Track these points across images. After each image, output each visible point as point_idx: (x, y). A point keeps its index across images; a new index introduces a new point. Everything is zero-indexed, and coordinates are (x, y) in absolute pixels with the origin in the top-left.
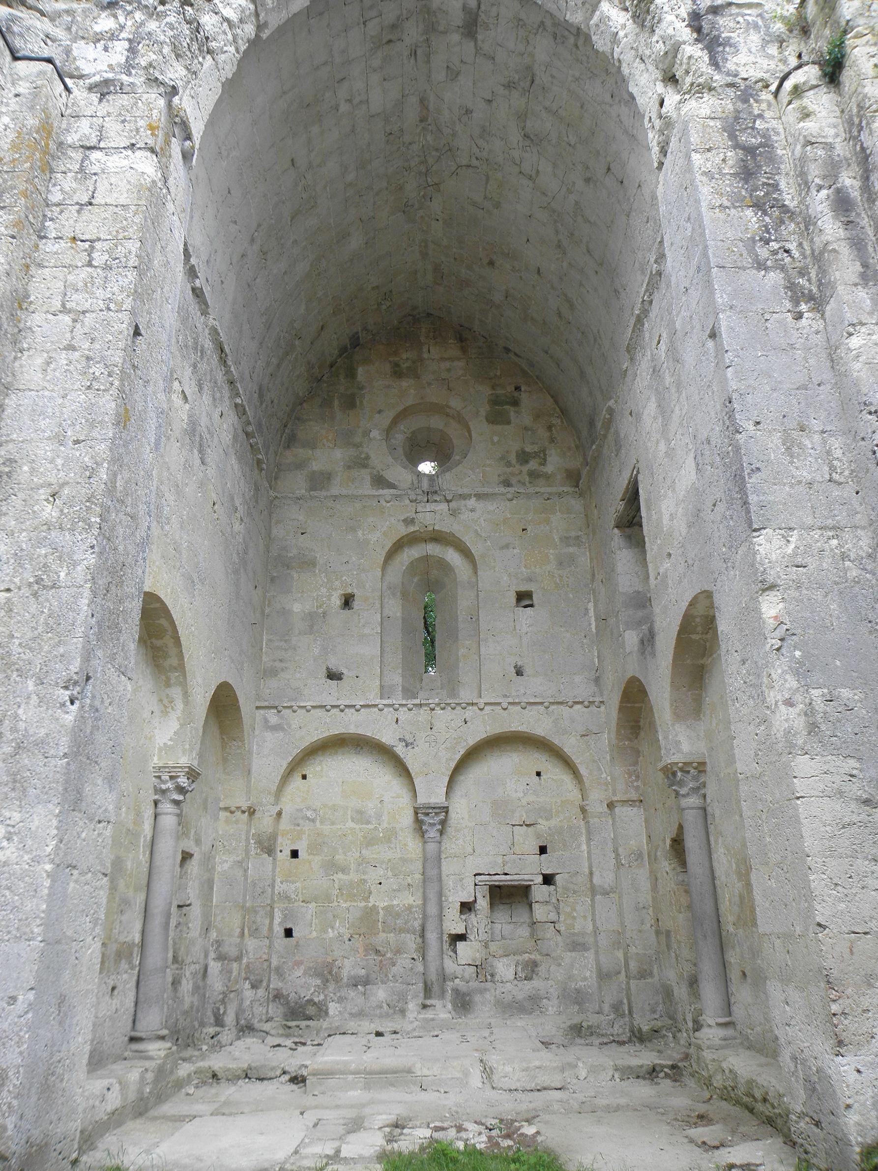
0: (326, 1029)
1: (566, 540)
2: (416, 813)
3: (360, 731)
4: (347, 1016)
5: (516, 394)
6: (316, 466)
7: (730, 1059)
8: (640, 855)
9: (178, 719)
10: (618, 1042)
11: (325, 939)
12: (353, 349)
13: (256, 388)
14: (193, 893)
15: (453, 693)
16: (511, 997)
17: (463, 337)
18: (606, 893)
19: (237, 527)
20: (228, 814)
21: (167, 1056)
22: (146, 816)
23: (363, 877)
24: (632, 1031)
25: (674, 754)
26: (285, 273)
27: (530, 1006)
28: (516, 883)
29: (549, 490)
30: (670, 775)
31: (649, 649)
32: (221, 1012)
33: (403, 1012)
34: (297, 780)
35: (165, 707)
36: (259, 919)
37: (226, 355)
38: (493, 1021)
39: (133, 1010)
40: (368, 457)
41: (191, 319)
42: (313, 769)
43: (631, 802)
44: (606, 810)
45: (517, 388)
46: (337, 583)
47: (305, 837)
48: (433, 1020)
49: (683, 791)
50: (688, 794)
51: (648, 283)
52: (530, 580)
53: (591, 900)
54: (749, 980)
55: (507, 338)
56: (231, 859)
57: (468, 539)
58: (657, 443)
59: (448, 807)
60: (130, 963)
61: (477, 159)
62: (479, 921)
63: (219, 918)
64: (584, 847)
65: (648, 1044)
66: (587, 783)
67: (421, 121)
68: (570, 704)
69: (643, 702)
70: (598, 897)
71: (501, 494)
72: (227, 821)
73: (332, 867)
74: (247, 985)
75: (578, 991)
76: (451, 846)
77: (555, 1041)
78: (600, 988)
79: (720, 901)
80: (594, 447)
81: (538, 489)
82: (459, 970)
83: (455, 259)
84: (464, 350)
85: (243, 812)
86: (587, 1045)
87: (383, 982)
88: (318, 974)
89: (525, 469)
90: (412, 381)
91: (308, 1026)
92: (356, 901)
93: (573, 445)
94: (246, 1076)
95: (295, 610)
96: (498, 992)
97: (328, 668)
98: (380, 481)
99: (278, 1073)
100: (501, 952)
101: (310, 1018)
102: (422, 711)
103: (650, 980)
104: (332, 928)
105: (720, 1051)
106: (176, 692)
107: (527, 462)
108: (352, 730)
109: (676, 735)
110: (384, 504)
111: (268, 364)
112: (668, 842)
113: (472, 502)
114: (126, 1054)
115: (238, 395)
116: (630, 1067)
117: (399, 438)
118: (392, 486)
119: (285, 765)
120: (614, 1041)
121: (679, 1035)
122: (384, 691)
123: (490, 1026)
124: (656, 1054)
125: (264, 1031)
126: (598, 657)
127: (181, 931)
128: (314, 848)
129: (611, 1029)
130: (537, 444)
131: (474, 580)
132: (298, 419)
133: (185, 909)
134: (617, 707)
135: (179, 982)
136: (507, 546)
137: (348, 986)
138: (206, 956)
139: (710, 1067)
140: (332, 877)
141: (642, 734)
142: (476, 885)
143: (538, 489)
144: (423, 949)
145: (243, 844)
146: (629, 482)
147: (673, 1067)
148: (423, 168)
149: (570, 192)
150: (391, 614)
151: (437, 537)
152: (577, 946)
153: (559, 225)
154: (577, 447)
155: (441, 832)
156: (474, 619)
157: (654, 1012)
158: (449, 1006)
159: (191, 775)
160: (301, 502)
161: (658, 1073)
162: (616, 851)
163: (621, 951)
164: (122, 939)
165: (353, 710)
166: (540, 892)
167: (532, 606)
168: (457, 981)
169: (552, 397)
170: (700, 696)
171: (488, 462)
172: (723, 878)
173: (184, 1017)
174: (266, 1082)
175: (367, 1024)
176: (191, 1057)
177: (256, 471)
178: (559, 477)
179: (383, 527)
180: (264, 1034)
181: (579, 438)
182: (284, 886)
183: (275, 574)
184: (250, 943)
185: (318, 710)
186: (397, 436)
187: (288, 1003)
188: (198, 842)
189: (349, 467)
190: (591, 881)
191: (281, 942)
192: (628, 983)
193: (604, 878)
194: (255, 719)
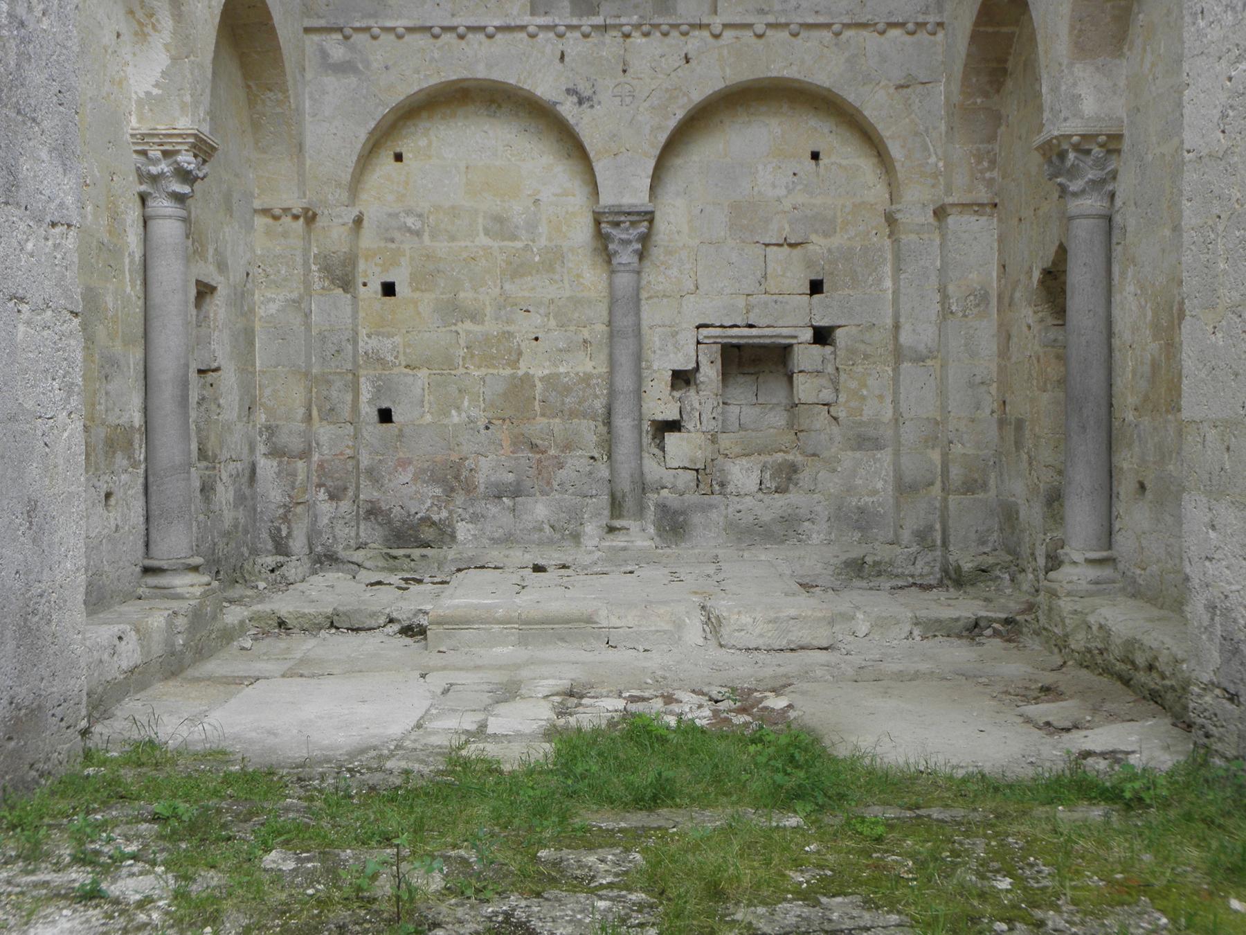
3: (496, 75)
4: (486, 541)
9: (166, 46)
10: (920, 586)
11: (446, 426)
14: (221, 350)
16: (751, 518)
18: (920, 359)
20: (270, 221)
21: (204, 595)
23: (507, 328)
24: (945, 571)
25: (1066, 119)
28: (768, 341)
30: (1054, 158)
32: (284, 534)
33: (576, 537)
34: (385, 166)
35: (141, 24)
36: (334, 394)
38: (720, 552)
39: (142, 527)
42: (414, 142)
43: (976, 208)
47: (404, 261)
48: (625, 549)
49: (1074, 187)
50: (1083, 191)
53: (894, 370)
54: (1149, 495)
56: (281, 297)
59: (652, 213)
60: (129, 458)
63: (268, 392)
64: (888, 284)
65: (969, 589)
66: (901, 173)
68: (881, 27)
70: (906, 366)
72: (268, 232)
73: (453, 311)
74: (322, 495)
75: (861, 511)
76: (656, 278)
78: (898, 505)
82: (668, 477)
85: (296, 217)
86: (871, 589)
87: (543, 493)
88: (435, 480)
92: (495, 367)
94: (332, 625)
96: (730, 510)
99: (382, 620)
101: (427, 545)
102: (607, 39)
103: (981, 496)
104: (458, 408)
108: (481, 72)
109: (1075, 85)
112: (1037, 275)
114: (140, 591)
123: (716, 560)
124: (981, 603)
128: (422, 280)
129: (912, 568)
133: (211, 377)
134: (968, 32)
135: (213, 489)
138: (252, 449)
139: (1067, 621)
140: (453, 328)
141: (1010, 84)
142: (698, 343)
144: (609, 444)
145: (299, 271)
147: (1007, 621)
152: (865, 441)
155: (641, 255)
158: (651, 530)
159: (200, 149)
162: (942, 290)
164: (112, 420)
165: (481, 36)
166: (807, 356)
168: (665, 492)
172: (1127, 336)
173: (225, 540)
174: (362, 633)
176: (242, 597)
182: (373, 342)
184: (322, 430)
185: (417, 36)
187: (390, 522)
188: (222, 267)
190: (896, 338)
191: (373, 430)
192: (945, 500)
193: (919, 333)
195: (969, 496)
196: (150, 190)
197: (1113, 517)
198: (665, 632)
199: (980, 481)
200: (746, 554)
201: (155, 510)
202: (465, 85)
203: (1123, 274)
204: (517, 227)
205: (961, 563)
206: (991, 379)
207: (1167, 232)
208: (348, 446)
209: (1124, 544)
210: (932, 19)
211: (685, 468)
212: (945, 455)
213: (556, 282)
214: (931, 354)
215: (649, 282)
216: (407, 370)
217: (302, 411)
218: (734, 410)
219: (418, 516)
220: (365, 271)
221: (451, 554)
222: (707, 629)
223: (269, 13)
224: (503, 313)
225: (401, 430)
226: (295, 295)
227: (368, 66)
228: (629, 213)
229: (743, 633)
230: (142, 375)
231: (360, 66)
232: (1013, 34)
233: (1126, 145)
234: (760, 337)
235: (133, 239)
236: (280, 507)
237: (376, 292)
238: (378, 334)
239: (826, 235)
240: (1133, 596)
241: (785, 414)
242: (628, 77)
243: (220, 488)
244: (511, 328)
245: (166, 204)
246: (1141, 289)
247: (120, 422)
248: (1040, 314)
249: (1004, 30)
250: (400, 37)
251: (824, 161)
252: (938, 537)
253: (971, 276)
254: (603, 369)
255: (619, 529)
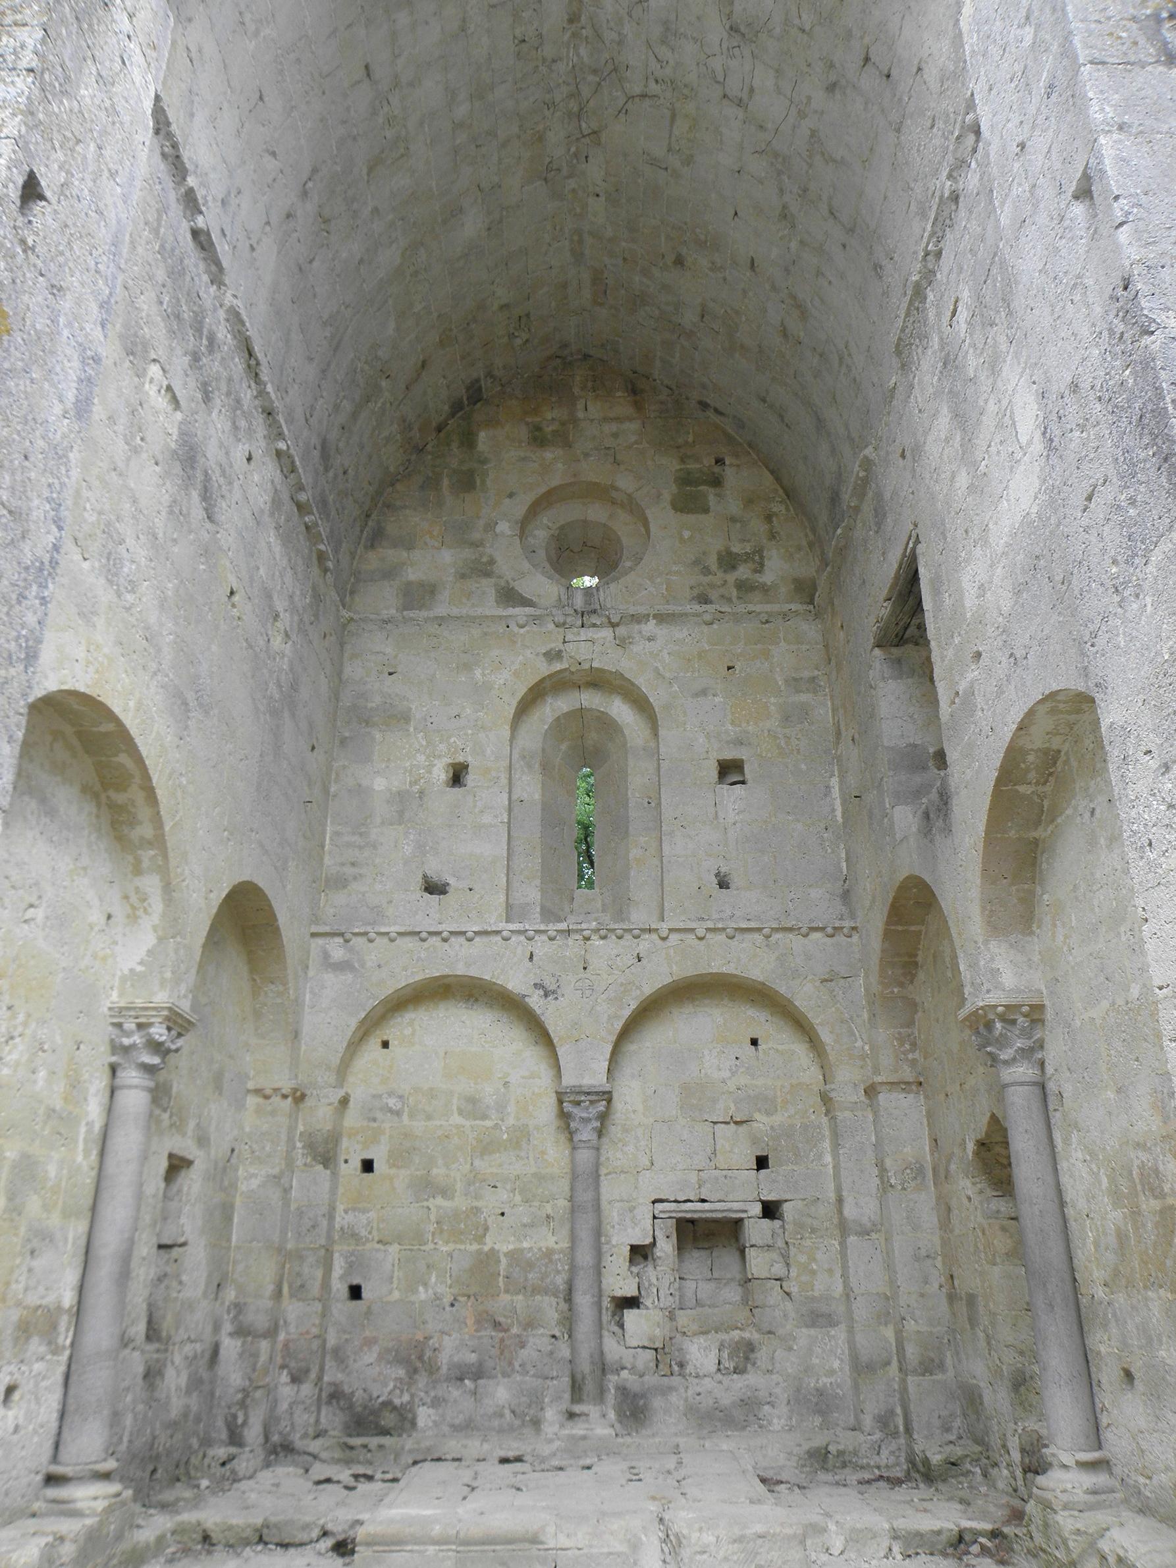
0: (410, 1451)
1: (795, 684)
2: (560, 1102)
3: (474, 972)
4: (446, 1429)
5: (717, 469)
6: (412, 575)
7: (1115, 1533)
8: (920, 1171)
9: (155, 928)
10: (888, 1479)
11: (413, 1303)
12: (470, 405)
13: (315, 440)
14: (190, 1223)
15: (620, 914)
16: (711, 1402)
17: (636, 389)
18: (864, 1232)
19: (277, 642)
20: (260, 1100)
21: (109, 1510)
22: (92, 1090)
23: (475, 1204)
24: (912, 1462)
25: (988, 991)
26: (361, 261)
27: (741, 1416)
28: (720, 1215)
29: (768, 608)
30: (982, 1029)
31: (940, 823)
32: (240, 1421)
33: (536, 1423)
34: (372, 1051)
35: (134, 908)
36: (306, 1270)
37: (258, 364)
38: (681, 1441)
39: (54, 1425)
40: (492, 562)
41: (188, 278)
42: (400, 1028)
43: (903, 1086)
44: (863, 1098)
45: (719, 461)
46: (442, 747)
47: (384, 1139)
48: (584, 1438)
49: (1005, 1055)
50: (1014, 1059)
51: (936, 219)
52: (739, 743)
53: (840, 1244)
54: (1139, 1385)
55: (704, 387)
56: (263, 1173)
57: (643, 682)
58: (953, 477)
59: (610, 1092)
60: (50, 1343)
61: (657, 82)
62: (659, 1276)
63: (240, 1267)
64: (828, 1159)
65: (941, 1486)
66: (832, 1056)
67: (571, 21)
68: (804, 931)
69: (923, 922)
70: (852, 1239)
71: (697, 615)
72: (259, 1111)
73: (427, 1187)
74: (284, 1377)
75: (820, 1392)
76: (615, 1155)
77: (784, 1477)
78: (856, 1387)
79: (1076, 1242)
80: (839, 531)
81: (751, 607)
82: (627, 1356)
83: (625, 259)
84: (638, 406)
85: (285, 1097)
86: (837, 1483)
87: (505, 1375)
88: (400, 1359)
89: (731, 577)
90: (559, 452)
91: (381, 1447)
92: (462, 1242)
93: (804, 543)
94: (261, 1540)
95: (376, 787)
96: (690, 1392)
97: (425, 876)
98: (510, 596)
99: (315, 1533)
100: (695, 1327)
101: (385, 1432)
102: (570, 942)
103: (939, 1377)
104: (425, 1285)
105: (1086, 1514)
106: (151, 884)
107: (734, 568)
108: (461, 970)
109: (992, 959)
110: (516, 629)
111: (337, 408)
112: (971, 1147)
113: (650, 627)
114: (37, 1506)
115: (281, 436)
116: (919, 1534)
117: (540, 535)
118: (526, 602)
119: (354, 1023)
120: (882, 1476)
121: (994, 1472)
122: (511, 912)
123: (677, 1451)
124: (959, 1507)
125: (309, 1454)
126: (847, 861)
127: (167, 1288)
128: (399, 1157)
129: (877, 1458)
130: (749, 541)
131: (653, 744)
132: (388, 507)
133: (175, 1252)
134: (881, 932)
135: (160, 1373)
136: (704, 692)
137: (448, 1379)
138: (217, 1328)
139: (1071, 1544)
140: (425, 1204)
141: (921, 976)
142: (654, 1217)
143: (751, 607)
144: (569, 1322)
145: (282, 1147)
146: (900, 567)
147: (994, 1534)
148: (574, 106)
149: (802, 115)
150: (525, 796)
151: (598, 681)
152: (818, 1318)
153: (785, 178)
154: (811, 545)
155: (600, 1133)
156: (654, 803)
157: (948, 1430)
158: (612, 1415)
159: (175, 1022)
160: (389, 626)
161: (968, 1545)
162: (880, 1165)
163: (891, 1328)
164: (32, 1299)
165: (462, 939)
166: (757, 1230)
167: (743, 782)
168: (625, 1374)
169: (772, 472)
170: (1032, 893)
171: (675, 568)
172: (1082, 1204)
173: (169, 1432)
174: (292, 1551)
175: (477, 1443)
176: (178, 1500)
177: (316, 571)
178: (783, 590)
179: (512, 668)
180: (310, 1459)
181: (814, 530)
182: (350, 1218)
183: (347, 734)
184: (290, 1308)
185: (408, 939)
186: (536, 532)
187: (351, 1406)
188: (202, 1141)
189: (463, 576)
190: (840, 1212)
191: (342, 1307)
192: (903, 1381)
193: (861, 1207)
194: (308, 952)
195: (928, 1378)
196: (121, 1061)
197: (1098, 1411)
198: (619, 1554)
199: (937, 1361)
200: (707, 1444)
201: (71, 1407)
202: (446, 981)
203: (1067, 1141)
204: (488, 1107)
205: (929, 1454)
206: (936, 1252)
207: (1111, 1094)
208: (314, 1325)
209: (1117, 1444)
210: (847, 924)
211: (644, 1347)
212: (899, 1333)
213: (522, 1158)
214: (874, 1228)
215: (608, 1159)
216: (380, 1246)
217: (270, 1288)
218: (690, 1286)
219: (380, 1400)
220: (347, 1149)
221: (409, 1444)
222: (666, 1550)
223: (275, 916)
224: (472, 1188)
225: (369, 1308)
226: (276, 1171)
227: (363, 966)
228: (588, 1093)
229: (705, 1556)
230: (84, 1250)
231: (356, 965)
232: (920, 931)
233: (1049, 1015)
234: (712, 1211)
235: (94, 1110)
236: (239, 1391)
237: (356, 1169)
238: (354, 1209)
239: (768, 1113)
240: (1141, 1511)
241: (740, 1289)
242: (588, 974)
243: (170, 1373)
244: (479, 1204)
245: (134, 1074)
246: (1090, 1155)
247: (44, 1302)
248: (979, 1186)
249: (913, 928)
250: (392, 940)
251: (762, 1046)
252: (900, 1422)
253: (905, 1150)
254: (565, 1244)
255: (579, 1415)
